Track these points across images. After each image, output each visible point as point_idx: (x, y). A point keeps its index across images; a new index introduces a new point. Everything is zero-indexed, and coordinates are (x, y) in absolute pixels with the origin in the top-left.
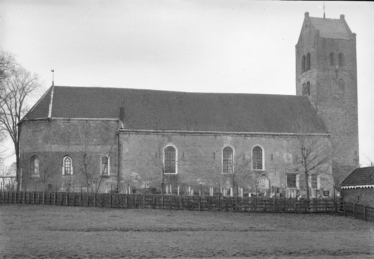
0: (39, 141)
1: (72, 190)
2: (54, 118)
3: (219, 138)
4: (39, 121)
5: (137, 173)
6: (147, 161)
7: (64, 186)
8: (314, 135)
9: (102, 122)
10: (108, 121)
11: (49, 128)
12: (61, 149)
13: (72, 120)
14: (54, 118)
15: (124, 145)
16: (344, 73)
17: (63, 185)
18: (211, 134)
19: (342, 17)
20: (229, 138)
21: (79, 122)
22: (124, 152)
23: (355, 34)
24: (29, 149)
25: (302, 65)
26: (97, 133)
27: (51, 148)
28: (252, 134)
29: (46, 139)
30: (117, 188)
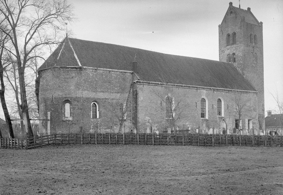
0: (71, 88)
1: (99, 131)
2: (85, 67)
3: (199, 91)
4: (70, 69)
5: (149, 118)
6: (155, 108)
7: (93, 128)
8: (250, 92)
9: (121, 73)
10: (125, 73)
11: (80, 76)
12: (91, 96)
13: (99, 70)
14: (85, 67)
15: (140, 93)
16: (257, 49)
17: (92, 127)
18: (194, 88)
19: (249, 9)
20: (205, 91)
21: (103, 72)
22: (140, 99)
23: (262, 22)
24: (61, 94)
25: (226, 40)
26: (117, 83)
27: (82, 94)
28: (218, 89)
29: (78, 86)
30: (132, 129)
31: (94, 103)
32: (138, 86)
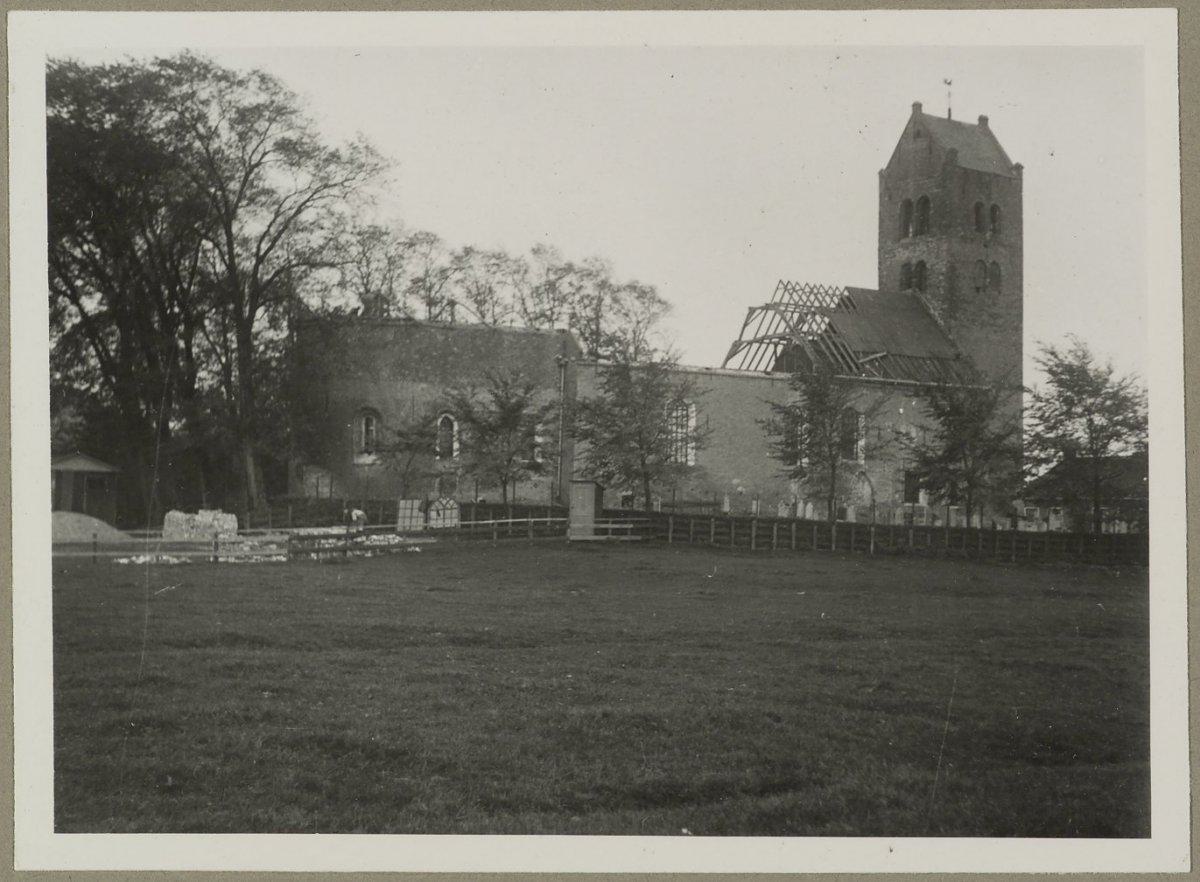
19: (983, 120)
31: (446, 418)
32: (579, 370)
